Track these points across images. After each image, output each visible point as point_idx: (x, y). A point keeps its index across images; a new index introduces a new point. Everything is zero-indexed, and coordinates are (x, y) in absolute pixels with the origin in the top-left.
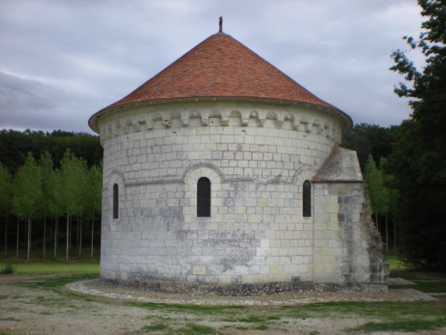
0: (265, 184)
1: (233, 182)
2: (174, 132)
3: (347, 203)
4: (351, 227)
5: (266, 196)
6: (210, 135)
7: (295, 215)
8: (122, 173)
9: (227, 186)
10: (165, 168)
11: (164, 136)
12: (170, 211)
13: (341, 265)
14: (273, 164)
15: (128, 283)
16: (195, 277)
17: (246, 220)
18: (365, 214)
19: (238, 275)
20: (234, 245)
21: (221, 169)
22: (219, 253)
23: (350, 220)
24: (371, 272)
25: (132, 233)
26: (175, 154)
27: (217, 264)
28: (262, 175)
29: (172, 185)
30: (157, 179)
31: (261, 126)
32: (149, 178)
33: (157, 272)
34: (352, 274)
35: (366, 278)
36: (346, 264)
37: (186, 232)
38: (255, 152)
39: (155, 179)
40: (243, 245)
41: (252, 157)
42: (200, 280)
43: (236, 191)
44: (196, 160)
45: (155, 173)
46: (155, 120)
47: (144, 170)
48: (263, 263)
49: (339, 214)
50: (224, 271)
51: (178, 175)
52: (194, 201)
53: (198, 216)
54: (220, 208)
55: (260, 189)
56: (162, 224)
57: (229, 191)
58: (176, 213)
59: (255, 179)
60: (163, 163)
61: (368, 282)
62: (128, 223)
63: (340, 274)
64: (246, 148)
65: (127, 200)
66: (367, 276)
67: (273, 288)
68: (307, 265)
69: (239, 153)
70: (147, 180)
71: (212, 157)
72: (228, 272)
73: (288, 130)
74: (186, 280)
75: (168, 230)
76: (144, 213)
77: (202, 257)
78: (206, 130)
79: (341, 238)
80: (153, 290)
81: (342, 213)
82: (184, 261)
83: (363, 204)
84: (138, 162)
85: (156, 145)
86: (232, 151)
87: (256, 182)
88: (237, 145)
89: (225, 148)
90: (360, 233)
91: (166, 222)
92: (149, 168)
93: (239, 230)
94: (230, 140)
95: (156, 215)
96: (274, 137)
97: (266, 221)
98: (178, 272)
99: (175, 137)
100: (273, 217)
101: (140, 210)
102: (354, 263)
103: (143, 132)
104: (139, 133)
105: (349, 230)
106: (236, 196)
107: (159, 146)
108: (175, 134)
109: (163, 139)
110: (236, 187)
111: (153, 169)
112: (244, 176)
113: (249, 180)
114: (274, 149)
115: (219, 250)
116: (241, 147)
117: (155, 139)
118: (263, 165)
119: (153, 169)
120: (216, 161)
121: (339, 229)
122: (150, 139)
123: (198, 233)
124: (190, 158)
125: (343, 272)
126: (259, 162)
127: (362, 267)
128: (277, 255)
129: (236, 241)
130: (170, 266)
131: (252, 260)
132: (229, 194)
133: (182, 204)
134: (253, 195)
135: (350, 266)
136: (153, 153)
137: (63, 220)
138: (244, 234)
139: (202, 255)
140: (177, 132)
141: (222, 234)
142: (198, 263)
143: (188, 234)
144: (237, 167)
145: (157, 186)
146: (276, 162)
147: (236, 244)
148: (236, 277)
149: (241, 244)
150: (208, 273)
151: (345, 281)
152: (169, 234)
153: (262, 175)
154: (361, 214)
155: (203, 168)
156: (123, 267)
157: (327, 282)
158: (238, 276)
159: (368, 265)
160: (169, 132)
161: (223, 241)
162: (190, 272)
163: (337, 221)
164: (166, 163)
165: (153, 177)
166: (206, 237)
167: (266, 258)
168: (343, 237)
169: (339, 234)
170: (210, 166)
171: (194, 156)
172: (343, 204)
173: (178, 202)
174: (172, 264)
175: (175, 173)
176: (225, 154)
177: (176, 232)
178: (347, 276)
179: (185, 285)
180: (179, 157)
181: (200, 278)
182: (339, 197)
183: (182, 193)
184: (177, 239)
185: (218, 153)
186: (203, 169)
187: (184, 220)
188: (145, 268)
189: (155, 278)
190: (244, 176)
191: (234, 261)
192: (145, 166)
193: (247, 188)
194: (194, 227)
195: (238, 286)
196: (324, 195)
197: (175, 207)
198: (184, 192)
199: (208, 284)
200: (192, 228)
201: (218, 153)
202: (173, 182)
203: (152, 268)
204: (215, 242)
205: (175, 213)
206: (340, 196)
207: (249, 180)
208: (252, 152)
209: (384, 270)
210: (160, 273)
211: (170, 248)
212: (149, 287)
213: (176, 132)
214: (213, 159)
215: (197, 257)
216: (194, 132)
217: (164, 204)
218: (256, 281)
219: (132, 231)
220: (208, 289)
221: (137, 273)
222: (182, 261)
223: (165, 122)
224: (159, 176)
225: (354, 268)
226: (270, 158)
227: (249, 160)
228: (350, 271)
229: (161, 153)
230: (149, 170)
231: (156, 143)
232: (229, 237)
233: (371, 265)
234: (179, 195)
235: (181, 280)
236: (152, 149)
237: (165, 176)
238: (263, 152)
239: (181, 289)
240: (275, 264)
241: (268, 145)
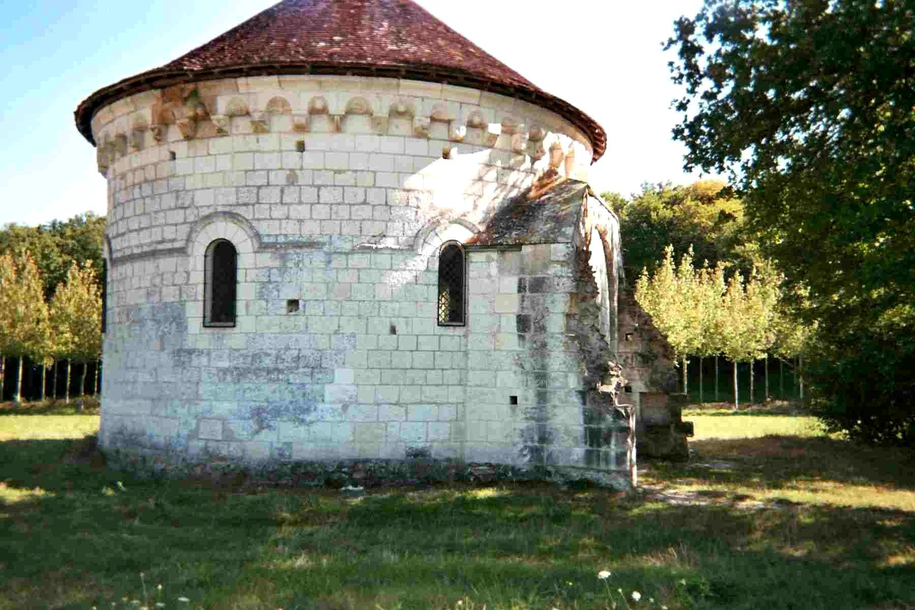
0: (347, 254)
1: (277, 249)
3: (537, 291)
4: (544, 345)
5: (347, 277)
7: (417, 317)
9: (266, 259)
13: (523, 425)
14: (366, 212)
16: (201, 444)
17: (302, 328)
18: (580, 317)
19: (284, 441)
20: (278, 379)
22: (247, 395)
23: (543, 329)
24: (586, 443)
27: (244, 419)
28: (340, 234)
31: (338, 129)
33: (144, 434)
34: (545, 445)
35: (576, 458)
36: (533, 423)
37: (190, 352)
38: (326, 186)
39: (146, 249)
40: (295, 379)
41: (318, 196)
42: (211, 450)
43: (283, 270)
45: (145, 238)
48: (339, 419)
49: (519, 317)
50: (257, 432)
55: (334, 264)
57: (270, 269)
59: (324, 244)
61: (581, 465)
63: (521, 446)
64: (304, 179)
67: (359, 470)
68: (449, 425)
69: (292, 188)
71: (237, 199)
72: (266, 436)
73: (405, 137)
79: (523, 368)
81: (525, 312)
82: (185, 411)
83: (571, 294)
87: (326, 249)
88: (288, 172)
89: (262, 181)
90: (562, 356)
93: (288, 348)
94: (272, 161)
96: (369, 153)
97: (348, 330)
98: (174, 434)
100: (363, 322)
102: (549, 422)
105: (541, 350)
110: (283, 258)
112: (301, 236)
113: (312, 245)
114: (368, 180)
115: (249, 388)
116: (296, 176)
118: (344, 212)
120: (244, 208)
121: (518, 348)
125: (525, 441)
126: (334, 208)
127: (567, 432)
128: (372, 401)
129: (280, 371)
131: (315, 410)
132: (269, 276)
133: (184, 297)
134: (319, 275)
137: (743, 365)
138: (298, 357)
141: (254, 356)
142: (208, 415)
143: (193, 356)
144: (288, 218)
146: (374, 206)
147: (281, 377)
148: (280, 445)
149: (291, 376)
150: (229, 436)
151: (530, 461)
153: (340, 234)
154: (568, 316)
157: (493, 462)
158: (285, 443)
159: (581, 429)
161: (257, 372)
163: (516, 331)
166: (225, 364)
167: (345, 407)
168: (527, 366)
169: (519, 358)
170: (231, 216)
171: (204, 199)
172: (528, 294)
176: (263, 192)
179: (184, 460)
181: (212, 445)
183: (185, 275)
185: (248, 191)
187: (186, 327)
189: (141, 445)
190: (301, 236)
191: (277, 412)
193: (307, 261)
194: (202, 345)
195: (284, 464)
198: (188, 273)
199: (223, 459)
201: (248, 191)
202: (171, 252)
204: (240, 374)
206: (521, 276)
207: (312, 245)
208: (319, 187)
209: (617, 440)
215: (207, 403)
217: (156, 298)
218: (322, 456)
225: (550, 433)
226: (361, 198)
227: (312, 204)
228: (543, 439)
229: (152, 197)
232: (267, 362)
233: (586, 429)
238: (343, 186)
240: (368, 420)
241: (356, 171)
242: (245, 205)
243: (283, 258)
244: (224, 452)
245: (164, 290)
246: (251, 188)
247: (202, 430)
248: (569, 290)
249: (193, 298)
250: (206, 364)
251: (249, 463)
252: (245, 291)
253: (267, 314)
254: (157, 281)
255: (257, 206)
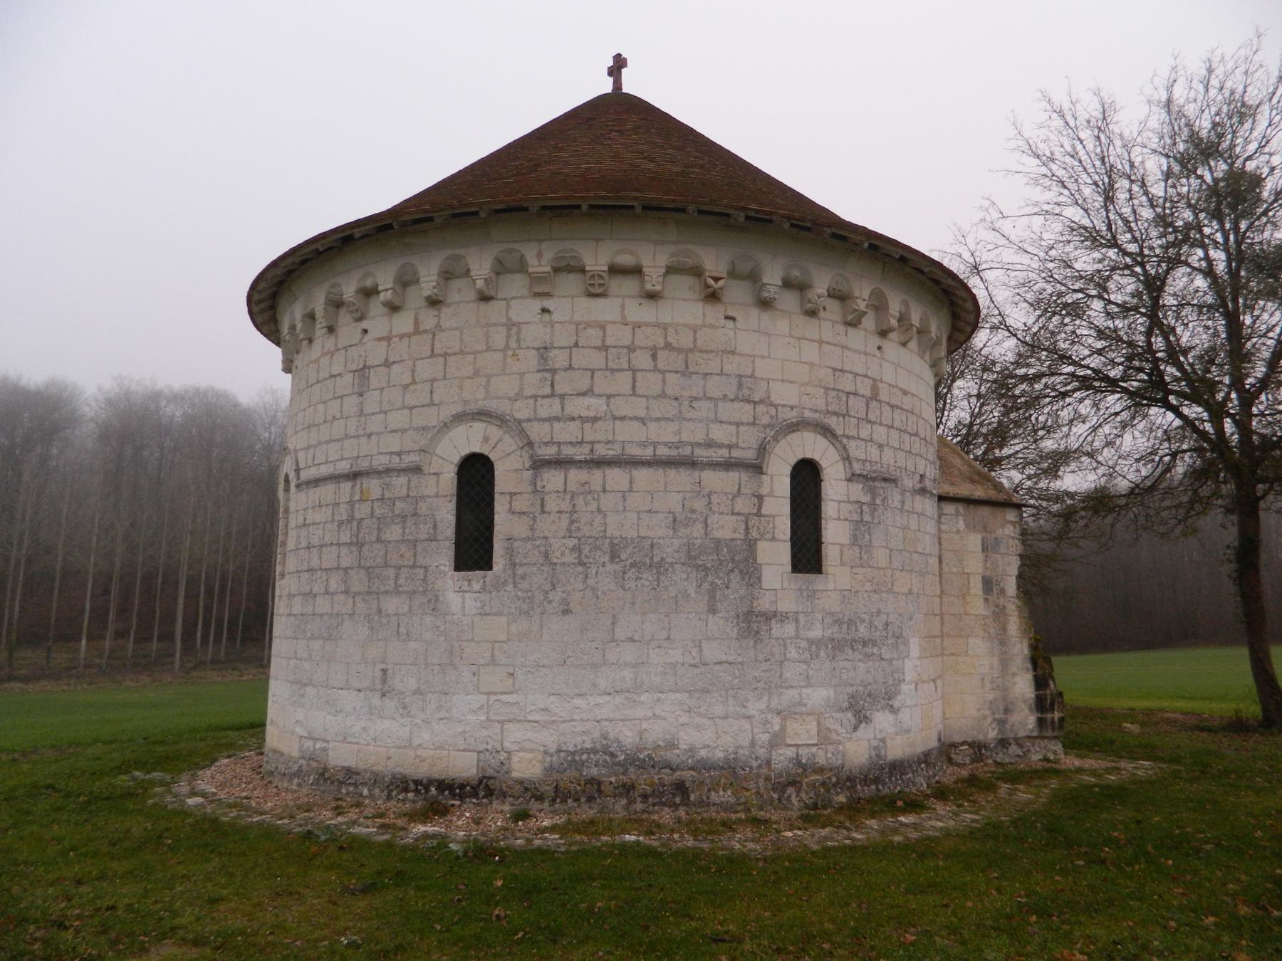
2: (727, 318)
6: (821, 342)
8: (519, 422)
10: (700, 421)
11: (699, 322)
12: (717, 550)
13: (990, 696)
15: (548, 789)
16: (791, 752)
21: (845, 440)
25: (568, 618)
26: (734, 382)
29: (722, 475)
30: (674, 453)
32: (643, 445)
37: (769, 616)
39: (663, 451)
44: (792, 408)
45: (666, 433)
46: (670, 270)
47: (623, 418)
51: (741, 445)
52: (783, 526)
53: (793, 571)
54: (845, 550)
56: (692, 591)
58: (737, 558)
60: (695, 404)
61: (1035, 734)
62: (547, 587)
63: (990, 720)
65: (543, 512)
66: (1032, 720)
70: (568, 451)
74: (768, 763)
75: (713, 610)
76: (624, 556)
77: (809, 691)
78: (811, 328)
80: (664, 804)
81: (988, 573)
84: (596, 390)
85: (668, 346)
86: (863, 396)
91: (706, 586)
92: (643, 415)
95: (671, 564)
98: (745, 741)
99: (731, 332)
101: (606, 547)
103: (617, 302)
104: (601, 301)
106: (873, 518)
107: (679, 350)
108: (730, 324)
109: (695, 333)
111: (658, 420)
117: (665, 327)
119: (658, 420)
120: (835, 418)
122: (647, 325)
123: (797, 620)
124: (775, 398)
125: (994, 714)
130: (719, 722)
133: (754, 534)
135: (1004, 699)
136: (656, 369)
139: (809, 685)
140: (738, 319)
142: (798, 709)
143: (773, 621)
145: (672, 473)
150: (824, 737)
152: (715, 622)
155: (808, 433)
156: (516, 735)
159: (1033, 696)
160: (714, 313)
162: (777, 740)
164: (705, 405)
165: (655, 445)
166: (816, 633)
170: (827, 432)
173: (743, 526)
174: (726, 717)
175: (734, 440)
177: (738, 616)
178: (1002, 723)
179: (767, 779)
180: (745, 392)
181: (804, 752)
182: (983, 539)
184: (741, 637)
186: (795, 438)
187: (759, 579)
188: (628, 737)
189: (669, 766)
192: (621, 407)
194: (787, 604)
196: (958, 532)
197: (732, 540)
198: (760, 498)
199: (821, 770)
200: (784, 606)
202: (728, 465)
203: (656, 733)
204: (838, 646)
205: (733, 560)
210: (683, 746)
211: (717, 667)
212: (645, 797)
213: (733, 319)
214: (828, 412)
215: (794, 692)
216: (782, 325)
217: (697, 531)
219: (566, 612)
220: (823, 784)
221: (595, 751)
222: (756, 707)
223: (711, 282)
224: (679, 445)
228: (1007, 710)
230: (642, 421)
231: (670, 340)
232: (863, 631)
234: (743, 505)
235: (755, 764)
236: (654, 356)
237: (699, 445)
239: (758, 793)
242: (835, 413)
243: (873, 492)
244: (821, 760)
245: (713, 519)
246: (841, 394)
247: (789, 731)
248: (1019, 552)
249: (768, 536)
250: (793, 634)
251: (851, 771)
252: (834, 532)
253: (862, 566)
254: (699, 504)
255: (847, 418)
